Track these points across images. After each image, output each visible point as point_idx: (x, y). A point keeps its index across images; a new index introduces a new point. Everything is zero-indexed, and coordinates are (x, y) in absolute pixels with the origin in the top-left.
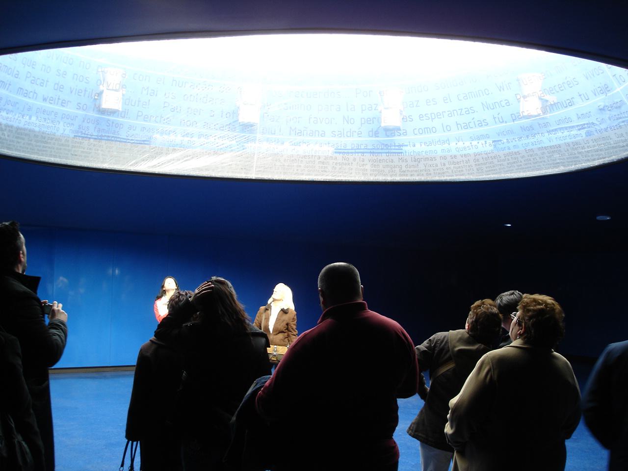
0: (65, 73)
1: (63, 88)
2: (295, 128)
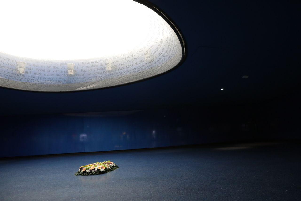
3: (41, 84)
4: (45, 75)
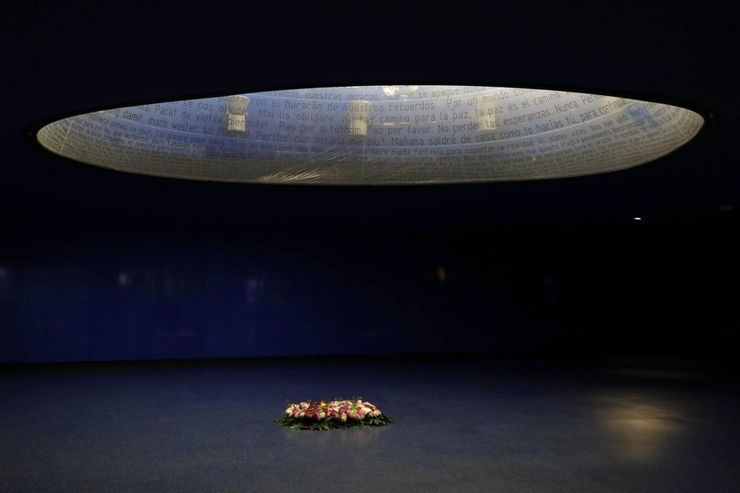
2: (397, 139)
3: (159, 153)
4: (174, 127)
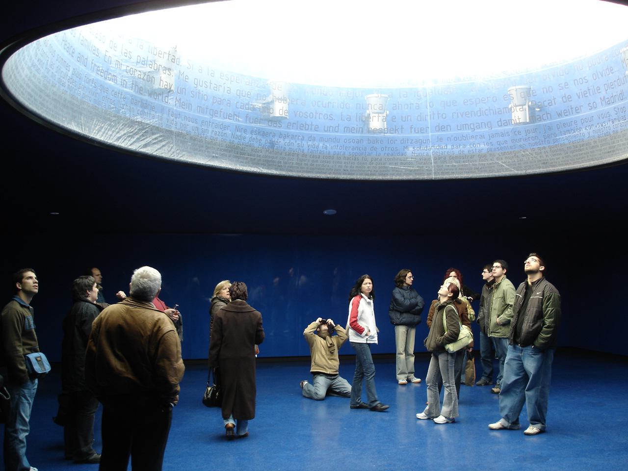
0: (566, 84)
1: (395, 118)
